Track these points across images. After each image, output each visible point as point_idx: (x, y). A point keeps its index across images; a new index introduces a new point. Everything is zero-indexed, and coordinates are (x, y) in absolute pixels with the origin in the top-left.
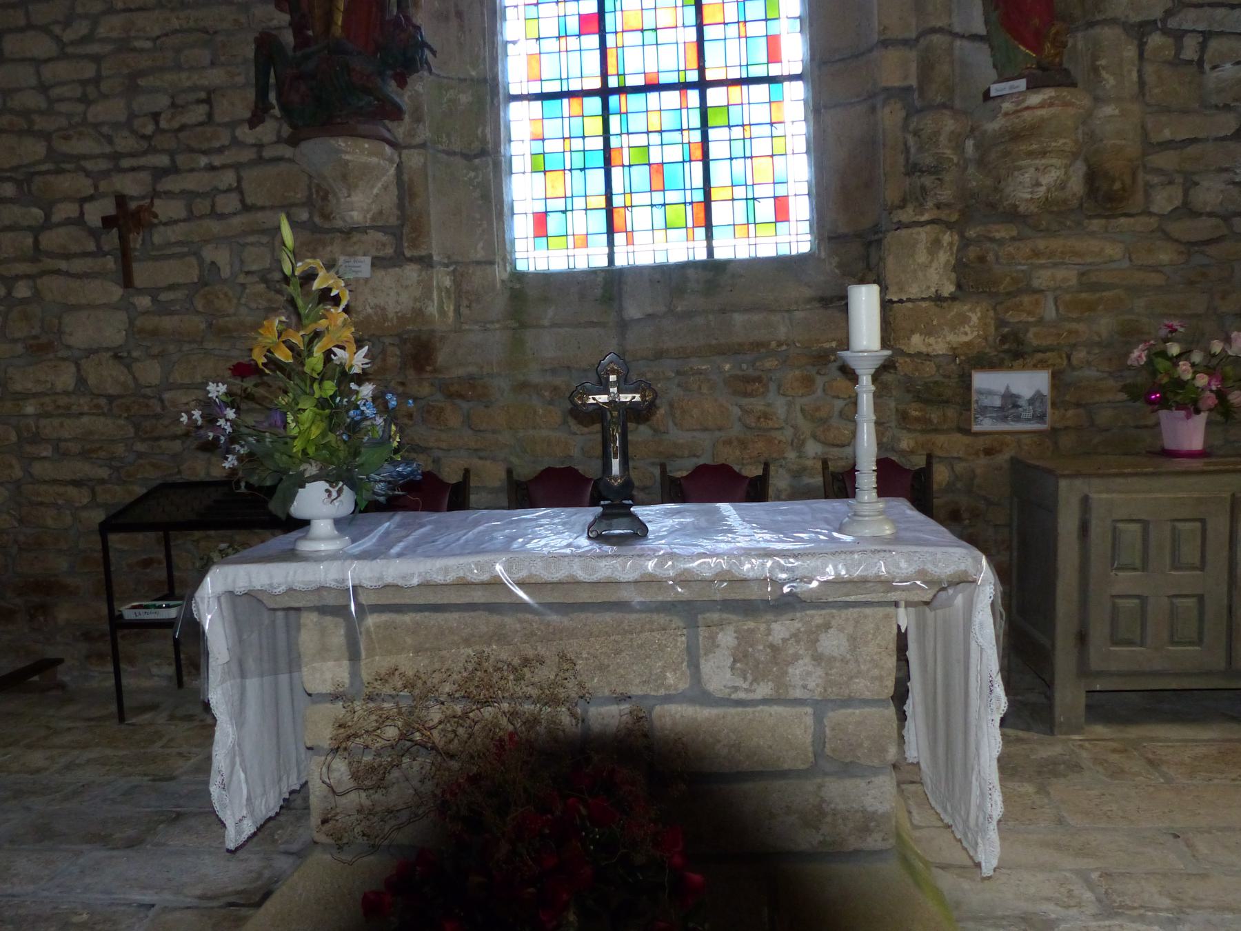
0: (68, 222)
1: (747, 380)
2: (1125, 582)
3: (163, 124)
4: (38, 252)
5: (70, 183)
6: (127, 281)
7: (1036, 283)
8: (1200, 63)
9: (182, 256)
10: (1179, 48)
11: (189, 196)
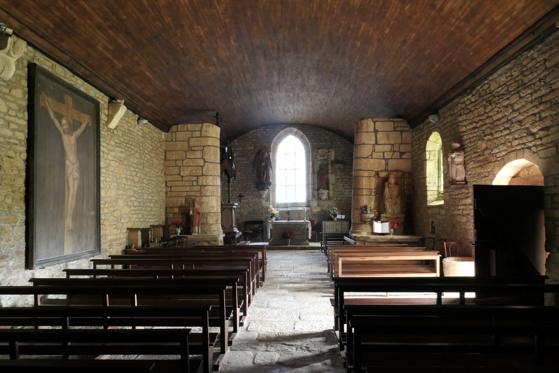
6: (240, 201)
11: (247, 194)
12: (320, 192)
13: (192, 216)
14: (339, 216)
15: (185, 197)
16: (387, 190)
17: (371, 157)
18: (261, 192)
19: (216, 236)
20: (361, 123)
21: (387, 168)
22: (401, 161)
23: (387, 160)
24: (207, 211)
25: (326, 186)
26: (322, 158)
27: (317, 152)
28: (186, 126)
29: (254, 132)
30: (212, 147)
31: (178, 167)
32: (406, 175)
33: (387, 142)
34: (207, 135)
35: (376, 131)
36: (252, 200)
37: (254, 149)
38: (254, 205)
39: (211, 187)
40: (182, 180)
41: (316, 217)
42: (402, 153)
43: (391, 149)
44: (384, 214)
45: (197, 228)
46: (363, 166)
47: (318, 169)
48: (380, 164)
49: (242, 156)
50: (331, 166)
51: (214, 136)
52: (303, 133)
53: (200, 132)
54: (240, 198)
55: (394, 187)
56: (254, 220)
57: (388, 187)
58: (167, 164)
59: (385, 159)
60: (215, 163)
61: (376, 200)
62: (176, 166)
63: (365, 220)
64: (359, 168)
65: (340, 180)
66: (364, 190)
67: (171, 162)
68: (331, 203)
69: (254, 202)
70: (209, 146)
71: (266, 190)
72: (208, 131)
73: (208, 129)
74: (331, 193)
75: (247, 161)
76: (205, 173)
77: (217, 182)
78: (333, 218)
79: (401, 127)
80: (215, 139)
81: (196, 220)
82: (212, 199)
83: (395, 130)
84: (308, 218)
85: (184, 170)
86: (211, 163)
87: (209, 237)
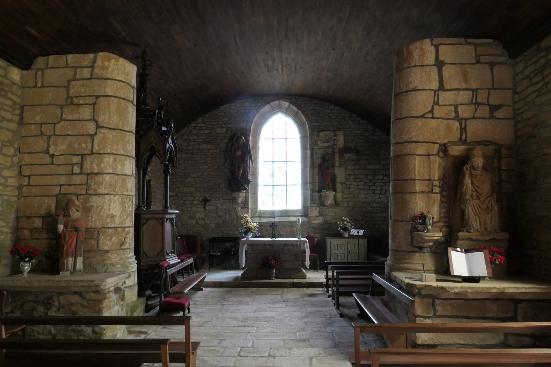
0: (197, 200)
1: (291, 226)
2: (335, 252)
3: (212, 187)
4: (192, 204)
5: (198, 194)
6: (205, 208)
7: (329, 215)
8: (349, 188)
9: (214, 205)
10: (347, 186)
11: (215, 198)
12: (323, 195)
13: (62, 235)
14: (354, 232)
15: (57, 196)
16: (468, 181)
17: (430, 116)
18: (235, 194)
19: (96, 282)
20: (407, 50)
21: (463, 138)
22: (492, 121)
23: (463, 122)
24: (98, 224)
25: (331, 186)
26: (326, 144)
27: (318, 136)
28: (64, 57)
29: (226, 108)
30: (113, 99)
31: (46, 138)
32: (504, 151)
33: (464, 86)
34: (105, 76)
35: (439, 64)
36: (222, 206)
37: (226, 132)
38: (226, 213)
39: (109, 176)
40: (52, 164)
41: (316, 231)
42: (494, 108)
43: (472, 99)
44: (463, 231)
45: (71, 260)
46: (414, 134)
47: (320, 161)
48: (449, 129)
49: (209, 142)
50: (339, 156)
51: (119, 78)
52: (298, 109)
53: (90, 69)
54: (205, 202)
55: (482, 175)
56: (225, 236)
57: (470, 176)
58: (23, 132)
59: (460, 120)
60: (120, 130)
61: (442, 202)
62: (42, 134)
63: (421, 245)
64: (406, 138)
65: (353, 177)
66: (417, 182)
67: (33, 126)
68: (339, 211)
69: (225, 209)
70: (107, 96)
71: (242, 191)
72: (107, 68)
73: (106, 63)
74: (339, 195)
75: (216, 149)
76: (97, 148)
77: (123, 168)
78: (342, 234)
79: (490, 55)
80: (121, 83)
81: (70, 243)
82: (110, 200)
83: (478, 62)
84: (305, 233)
85: (55, 144)
86: (111, 129)
87: (81, 284)
